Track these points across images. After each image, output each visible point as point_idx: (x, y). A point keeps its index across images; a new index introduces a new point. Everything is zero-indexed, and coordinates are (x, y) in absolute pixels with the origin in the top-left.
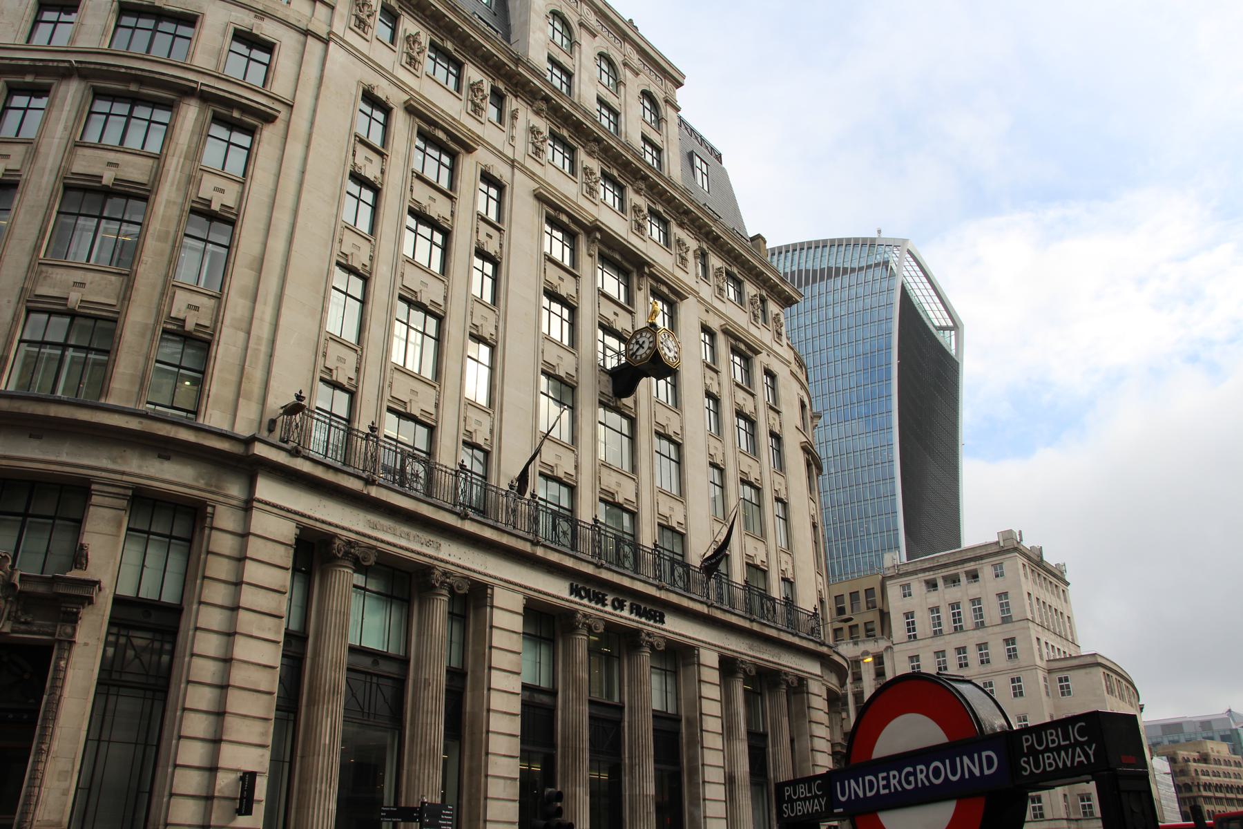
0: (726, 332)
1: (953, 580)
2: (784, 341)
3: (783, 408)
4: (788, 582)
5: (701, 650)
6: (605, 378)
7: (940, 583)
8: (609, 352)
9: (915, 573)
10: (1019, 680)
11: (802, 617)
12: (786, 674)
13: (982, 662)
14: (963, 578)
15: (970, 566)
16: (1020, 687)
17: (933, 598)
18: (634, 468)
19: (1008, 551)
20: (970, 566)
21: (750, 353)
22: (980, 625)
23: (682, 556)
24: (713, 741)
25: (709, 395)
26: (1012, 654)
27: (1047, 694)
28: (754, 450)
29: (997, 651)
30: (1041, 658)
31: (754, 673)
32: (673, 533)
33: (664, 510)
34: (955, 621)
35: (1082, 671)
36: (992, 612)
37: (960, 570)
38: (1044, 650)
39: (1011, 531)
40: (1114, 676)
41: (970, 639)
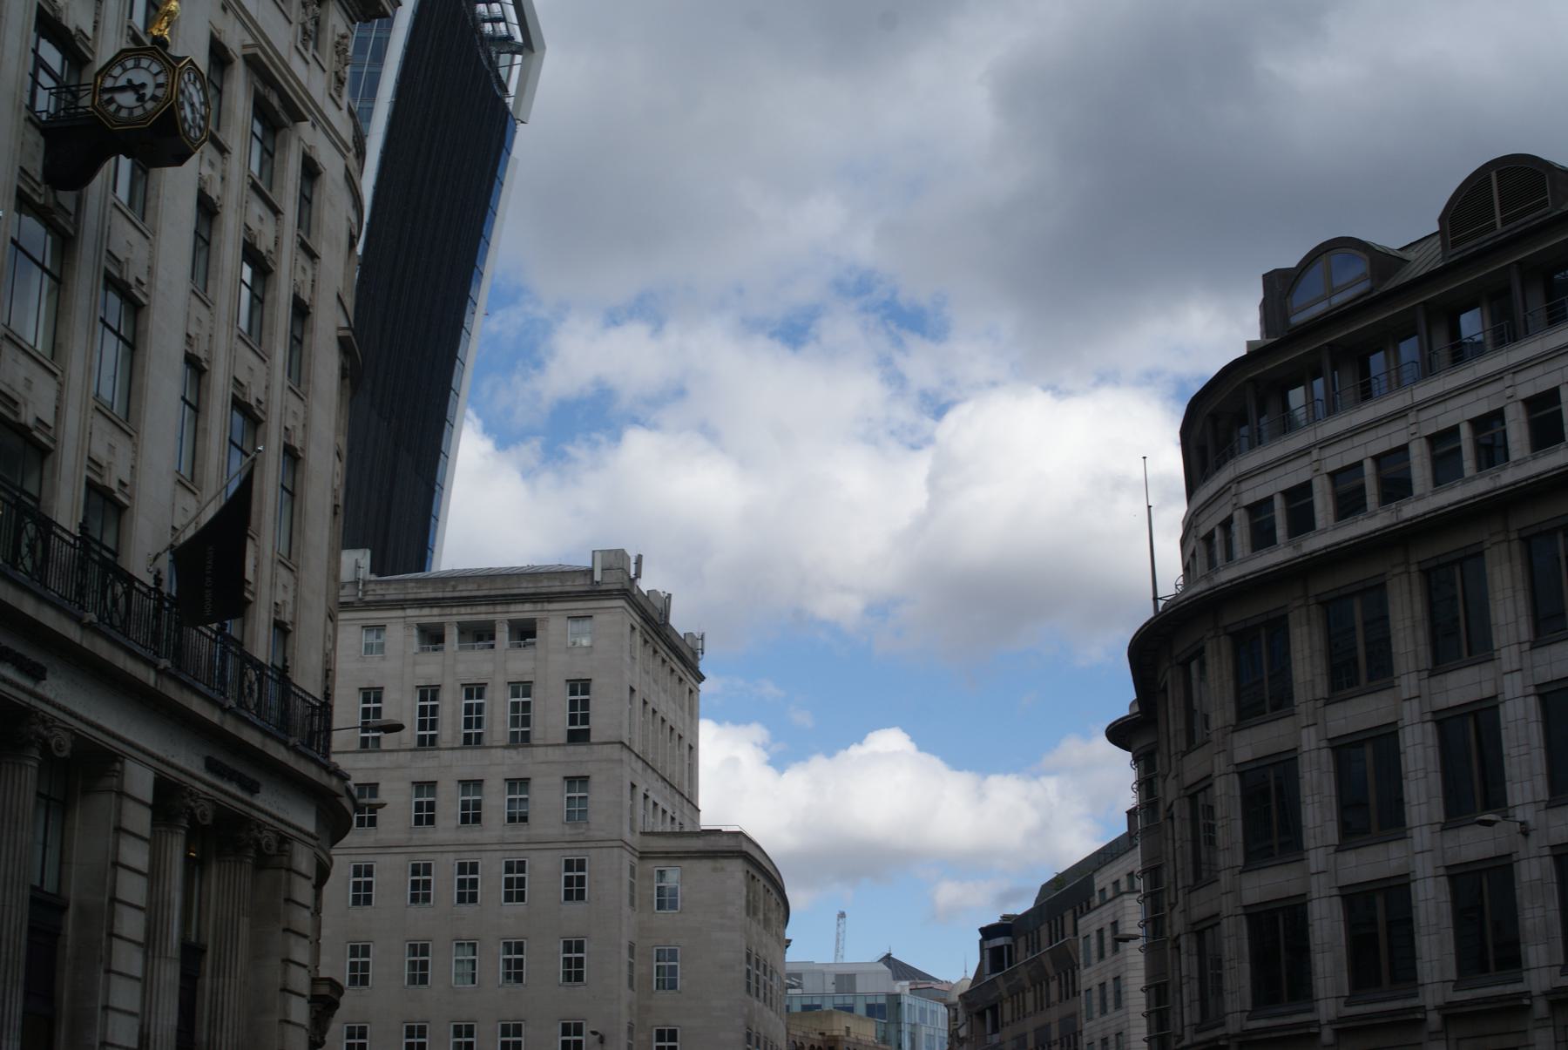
0: (252, 62)
1: (480, 634)
2: (345, 100)
3: (323, 249)
4: (282, 630)
5: (129, 764)
6: (34, 137)
7: (452, 636)
8: (44, 79)
9: (400, 604)
10: (581, 865)
11: (299, 708)
12: (260, 826)
13: (511, 819)
14: (503, 635)
15: (523, 611)
16: (581, 880)
17: (430, 668)
18: (56, 347)
19: (607, 594)
20: (523, 611)
21: (284, 117)
22: (521, 739)
23: (116, 554)
24: (128, 959)
25: (312, 255)
26: (577, 812)
27: (632, 903)
28: (254, 337)
29: (548, 798)
30: (632, 830)
31: (208, 821)
32: (106, 502)
33: (100, 451)
34: (468, 724)
35: (706, 865)
36: (551, 717)
37: (501, 617)
38: (640, 811)
39: (621, 554)
40: (763, 881)
41: (496, 765)
